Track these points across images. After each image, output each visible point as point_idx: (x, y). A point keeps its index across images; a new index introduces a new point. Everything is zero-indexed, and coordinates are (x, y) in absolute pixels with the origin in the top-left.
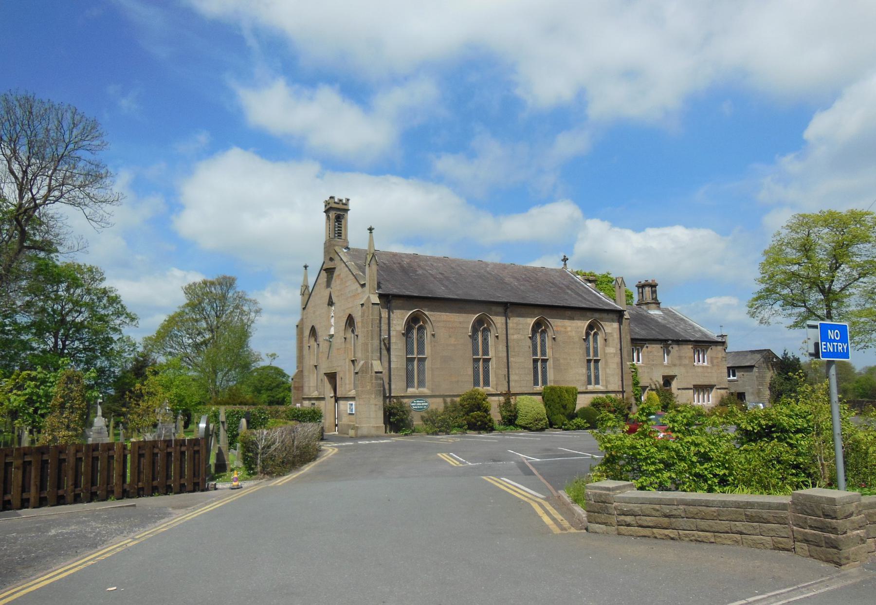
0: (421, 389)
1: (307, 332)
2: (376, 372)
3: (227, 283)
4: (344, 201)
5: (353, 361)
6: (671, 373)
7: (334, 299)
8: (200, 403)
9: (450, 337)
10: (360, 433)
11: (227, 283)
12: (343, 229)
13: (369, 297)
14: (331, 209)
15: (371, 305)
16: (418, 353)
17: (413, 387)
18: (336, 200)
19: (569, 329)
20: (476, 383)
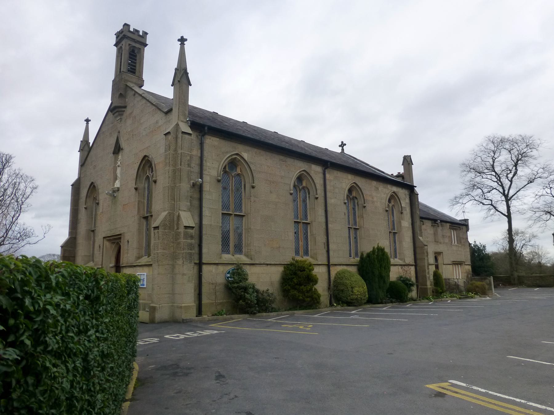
0: (238, 256)
1: (84, 192)
2: (186, 227)
3: (11, 157)
4: (141, 34)
5: (146, 218)
6: (439, 250)
7: (123, 144)
8: (297, 284)
9: (271, 192)
10: (158, 316)
11: (11, 157)
12: (137, 65)
13: (177, 125)
14: (125, 37)
15: (180, 135)
16: (236, 210)
17: (228, 252)
18: (131, 30)
19: (375, 199)
20: (297, 253)
